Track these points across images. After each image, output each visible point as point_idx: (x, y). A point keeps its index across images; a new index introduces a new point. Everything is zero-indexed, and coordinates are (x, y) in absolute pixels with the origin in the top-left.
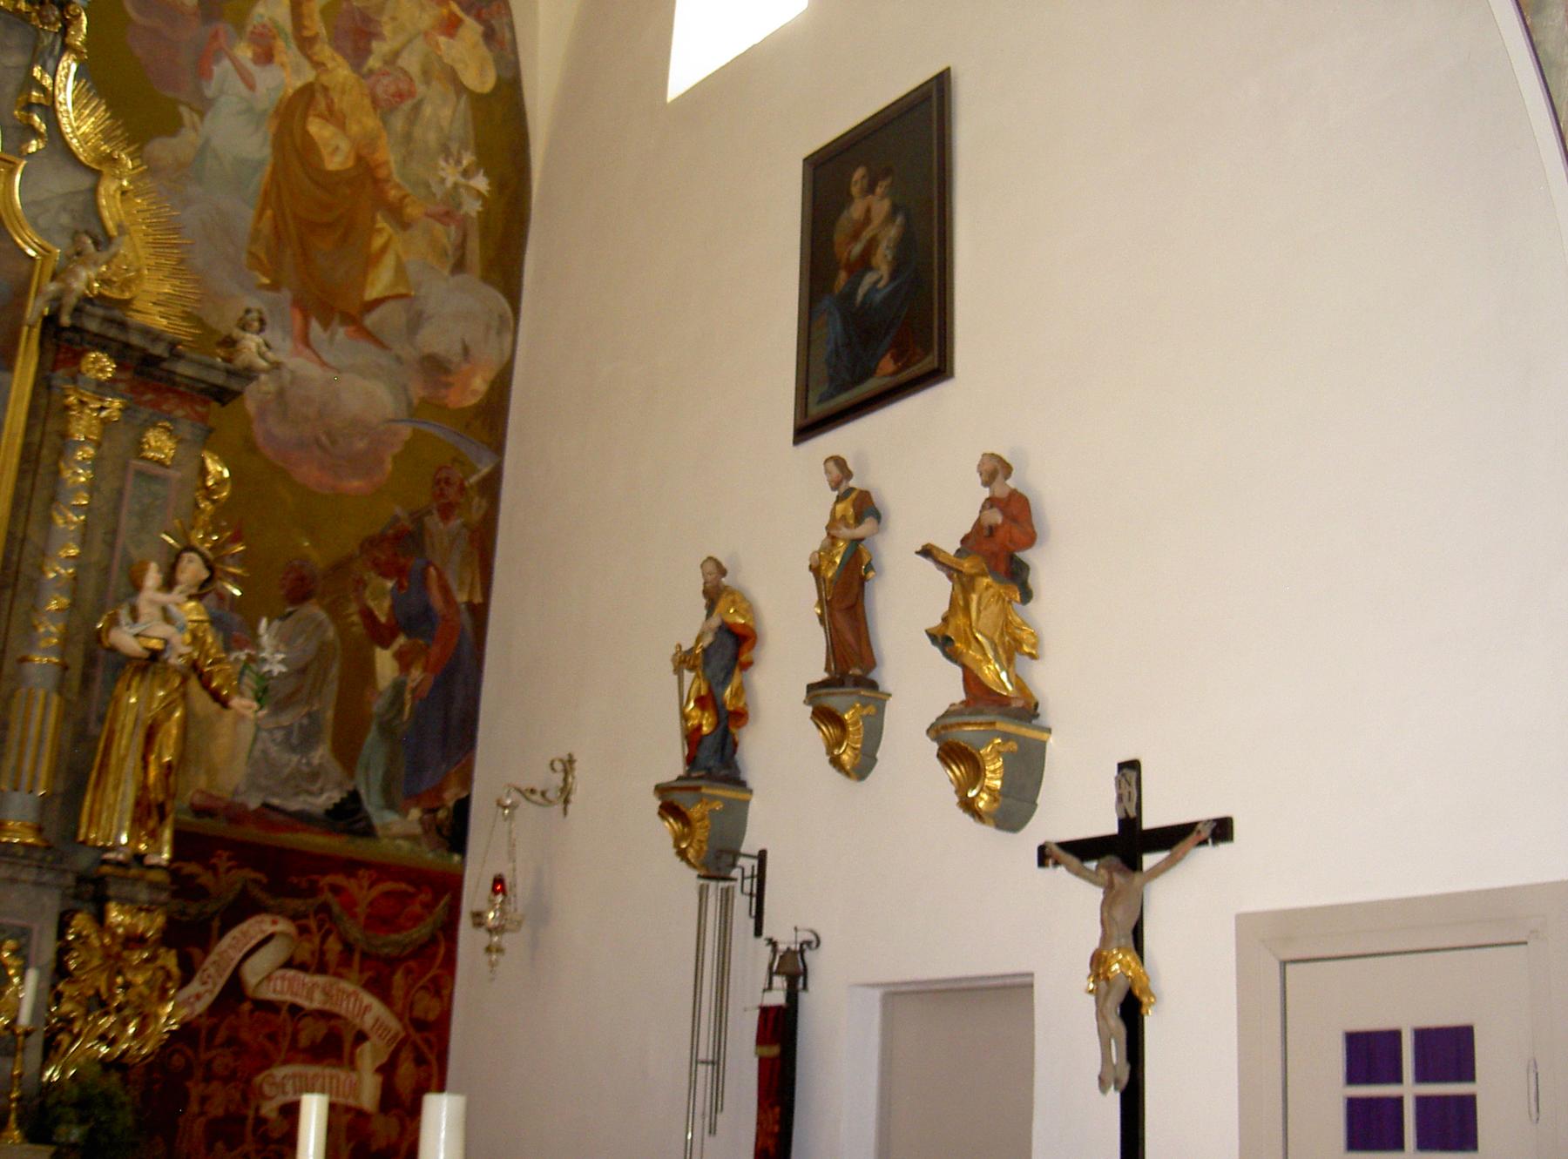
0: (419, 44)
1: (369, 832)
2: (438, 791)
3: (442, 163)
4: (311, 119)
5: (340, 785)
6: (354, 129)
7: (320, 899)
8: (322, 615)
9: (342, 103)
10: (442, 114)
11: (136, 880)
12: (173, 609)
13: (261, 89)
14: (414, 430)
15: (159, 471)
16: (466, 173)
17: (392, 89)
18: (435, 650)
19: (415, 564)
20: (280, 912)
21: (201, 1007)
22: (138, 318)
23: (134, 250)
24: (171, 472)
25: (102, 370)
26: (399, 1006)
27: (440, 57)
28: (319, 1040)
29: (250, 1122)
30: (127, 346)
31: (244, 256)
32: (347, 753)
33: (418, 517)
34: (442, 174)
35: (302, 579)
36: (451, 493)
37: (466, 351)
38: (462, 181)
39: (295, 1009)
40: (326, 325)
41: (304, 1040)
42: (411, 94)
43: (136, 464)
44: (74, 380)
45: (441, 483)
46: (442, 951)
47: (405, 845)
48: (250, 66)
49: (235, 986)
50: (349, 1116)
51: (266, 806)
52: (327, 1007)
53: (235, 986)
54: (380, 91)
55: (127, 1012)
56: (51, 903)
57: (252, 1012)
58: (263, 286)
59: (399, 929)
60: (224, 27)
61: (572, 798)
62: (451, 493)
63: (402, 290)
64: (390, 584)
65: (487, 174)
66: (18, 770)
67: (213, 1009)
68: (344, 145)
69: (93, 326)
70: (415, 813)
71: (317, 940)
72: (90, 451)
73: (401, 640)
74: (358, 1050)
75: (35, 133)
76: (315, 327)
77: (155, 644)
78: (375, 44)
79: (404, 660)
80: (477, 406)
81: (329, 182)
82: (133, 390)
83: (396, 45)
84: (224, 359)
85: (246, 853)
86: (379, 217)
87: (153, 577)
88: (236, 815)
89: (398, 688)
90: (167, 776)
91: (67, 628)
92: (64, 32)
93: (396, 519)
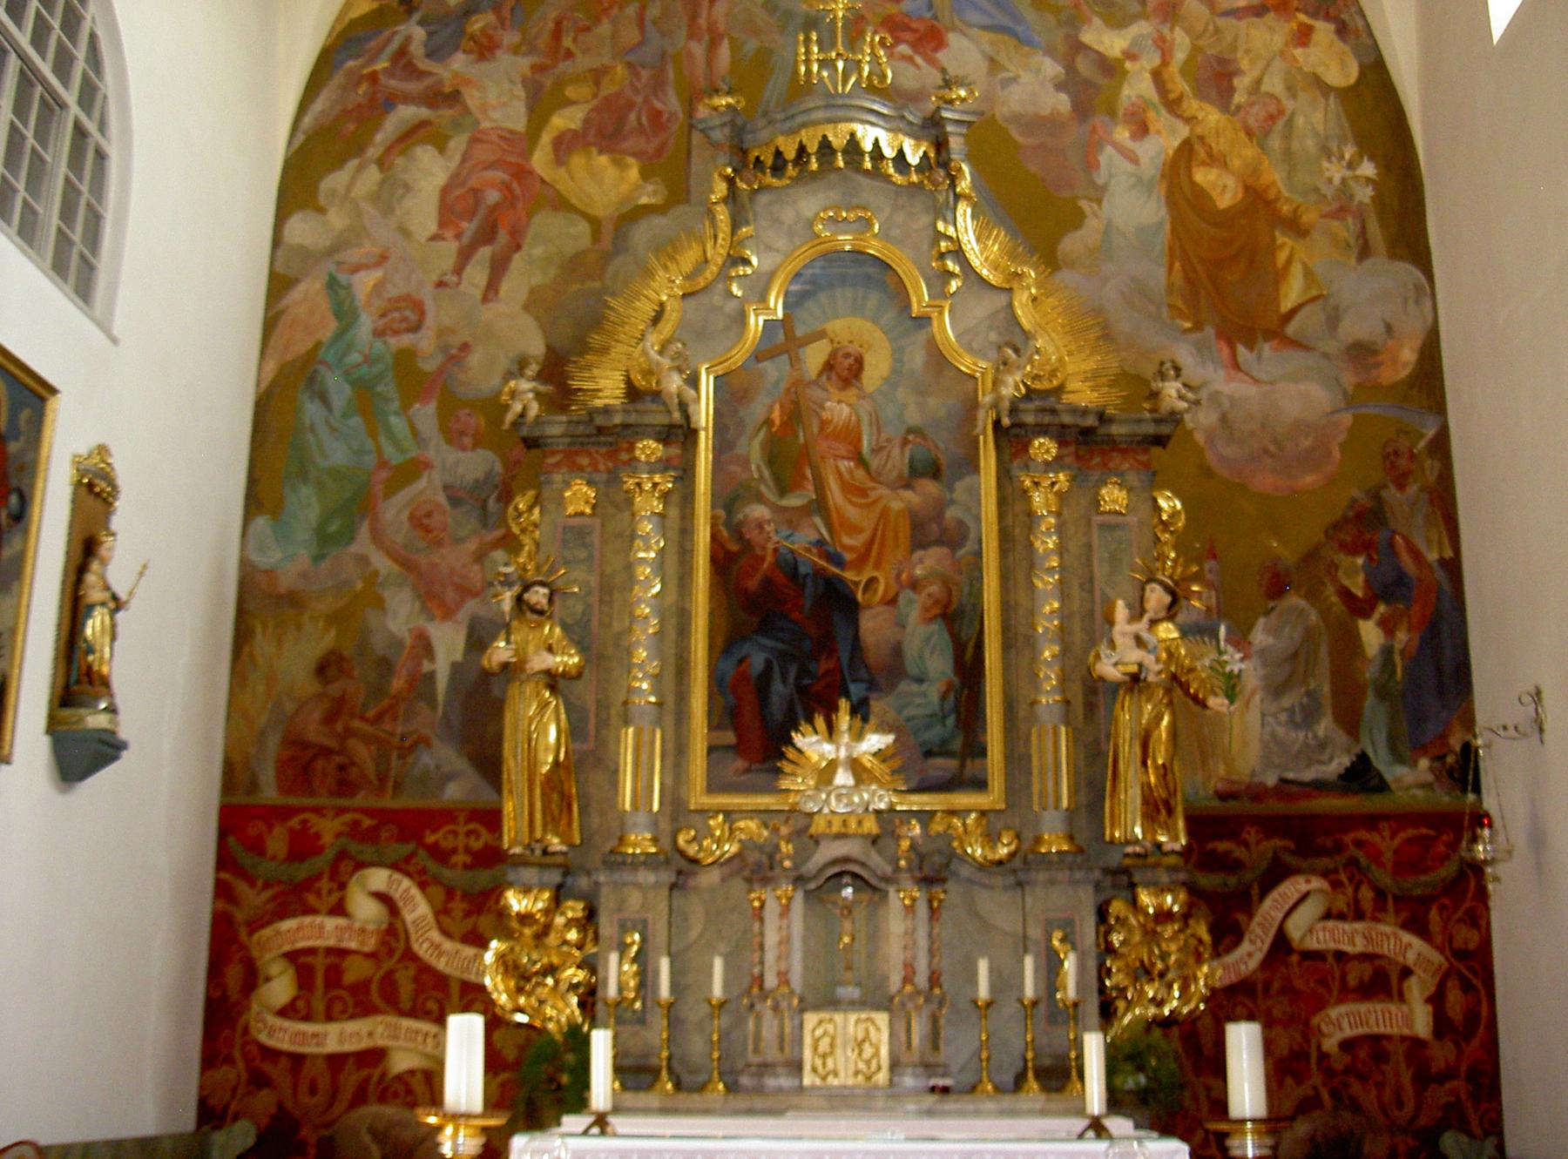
0: (1278, 64)
1: (1382, 787)
2: (1443, 738)
3: (1326, 165)
4: (1194, 170)
5: (1348, 751)
6: (1236, 163)
7: (1347, 855)
8: (1302, 603)
9: (1220, 145)
10: (1314, 119)
11: (1157, 865)
12: (1145, 635)
13: (1144, 160)
14: (1356, 417)
15: (1120, 519)
16: (1351, 166)
17: (1263, 114)
18: (1416, 609)
19: (1381, 537)
20: (1313, 871)
21: (1253, 964)
22: (1067, 398)
23: (1049, 346)
24: (1128, 519)
25: (1048, 451)
26: (1438, 939)
27: (1300, 69)
28: (1366, 979)
29: (1314, 1055)
30: (1063, 426)
31: (1165, 312)
32: (1350, 721)
33: (1376, 496)
34: (1327, 174)
35: (1277, 575)
36: (1403, 462)
37: (1389, 328)
38: (1349, 174)
39: (1340, 956)
40: (1251, 346)
41: (1352, 980)
42: (1281, 112)
43: (1098, 519)
44: (1027, 467)
45: (1390, 458)
46: (1473, 884)
47: (1420, 793)
48: (1130, 144)
49: (1281, 942)
50: (1406, 1045)
51: (1283, 781)
52: (1370, 949)
53: (1281, 942)
54: (1252, 122)
55: (1170, 976)
56: (1086, 900)
57: (1300, 964)
58: (1186, 331)
59: (1425, 871)
60: (1099, 120)
61: (1546, 727)
62: (1403, 462)
63: (1314, 292)
64: (1360, 561)
65: (1372, 158)
66: (1043, 794)
67: (1267, 963)
68: (1230, 182)
69: (1030, 419)
70: (1424, 763)
71: (1350, 891)
72: (1052, 520)
73: (1381, 608)
74: (1406, 984)
75: (952, 275)
76: (1241, 350)
77: (1134, 669)
78: (1236, 82)
79: (1387, 626)
80: (1410, 376)
81: (1226, 219)
82: (1078, 457)
83: (1256, 73)
84: (1150, 411)
85: (1272, 825)
86: (1277, 234)
87: (1121, 611)
88: (1257, 793)
89: (1387, 652)
90: (1165, 775)
91: (1063, 670)
92: (953, 185)
93: (1354, 501)
